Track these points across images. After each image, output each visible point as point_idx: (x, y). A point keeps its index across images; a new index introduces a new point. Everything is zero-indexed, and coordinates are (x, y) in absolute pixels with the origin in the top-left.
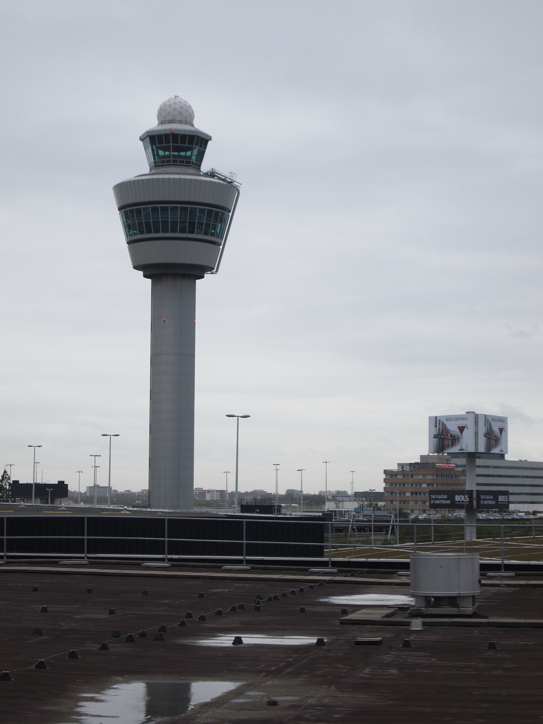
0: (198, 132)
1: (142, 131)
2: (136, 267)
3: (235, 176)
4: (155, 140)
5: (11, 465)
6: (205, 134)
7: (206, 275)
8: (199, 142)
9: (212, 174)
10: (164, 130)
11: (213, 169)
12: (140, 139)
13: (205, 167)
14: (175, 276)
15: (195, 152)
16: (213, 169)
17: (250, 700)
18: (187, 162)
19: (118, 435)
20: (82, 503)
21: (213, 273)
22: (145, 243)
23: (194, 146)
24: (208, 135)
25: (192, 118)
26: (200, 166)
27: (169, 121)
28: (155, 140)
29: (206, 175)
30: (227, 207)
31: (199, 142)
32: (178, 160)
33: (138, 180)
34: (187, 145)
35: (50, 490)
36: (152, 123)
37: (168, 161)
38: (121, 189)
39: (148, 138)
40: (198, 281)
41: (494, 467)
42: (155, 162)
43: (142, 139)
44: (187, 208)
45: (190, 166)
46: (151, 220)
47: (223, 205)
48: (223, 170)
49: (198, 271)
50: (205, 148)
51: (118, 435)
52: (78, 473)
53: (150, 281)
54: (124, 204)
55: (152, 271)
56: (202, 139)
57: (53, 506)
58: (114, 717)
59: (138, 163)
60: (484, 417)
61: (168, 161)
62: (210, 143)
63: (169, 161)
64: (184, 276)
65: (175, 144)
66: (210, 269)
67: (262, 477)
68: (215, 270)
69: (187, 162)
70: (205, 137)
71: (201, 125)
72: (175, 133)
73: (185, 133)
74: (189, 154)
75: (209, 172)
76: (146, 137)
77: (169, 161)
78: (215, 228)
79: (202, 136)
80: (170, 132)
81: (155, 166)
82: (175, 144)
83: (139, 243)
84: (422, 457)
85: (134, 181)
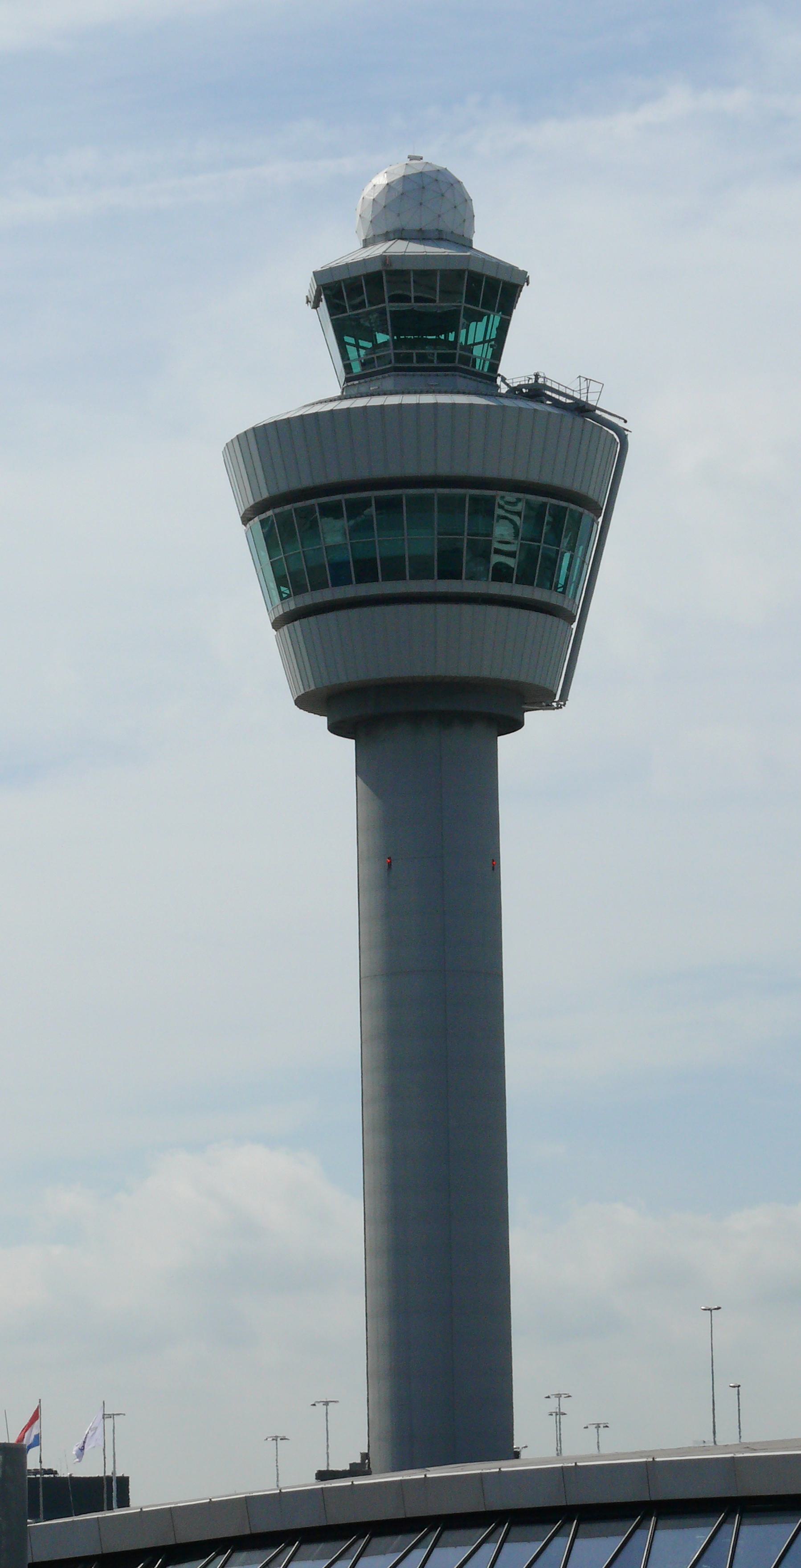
0: (487, 260)
2: (305, 702)
4: (346, 297)
6: (499, 265)
7: (529, 716)
8: (496, 292)
9: (535, 391)
11: (537, 376)
13: (515, 368)
14: (417, 718)
18: (442, 358)
22: (366, 611)
24: (512, 269)
25: (468, 218)
28: (346, 297)
29: (515, 392)
30: (590, 494)
31: (496, 292)
33: (316, 415)
36: (344, 244)
40: (503, 741)
45: (455, 369)
46: (465, 537)
48: (564, 379)
49: (504, 704)
51: (719, 1308)
52: (321, 1408)
53: (349, 745)
54: (275, 492)
55: (345, 704)
56: (493, 284)
64: (447, 719)
65: (418, 304)
66: (545, 698)
67: (582, 1448)
70: (504, 276)
71: (494, 239)
72: (397, 266)
73: (354, 274)
75: (525, 386)
78: (552, 563)
80: (378, 267)
82: (418, 304)
83: (331, 616)
85: (302, 417)
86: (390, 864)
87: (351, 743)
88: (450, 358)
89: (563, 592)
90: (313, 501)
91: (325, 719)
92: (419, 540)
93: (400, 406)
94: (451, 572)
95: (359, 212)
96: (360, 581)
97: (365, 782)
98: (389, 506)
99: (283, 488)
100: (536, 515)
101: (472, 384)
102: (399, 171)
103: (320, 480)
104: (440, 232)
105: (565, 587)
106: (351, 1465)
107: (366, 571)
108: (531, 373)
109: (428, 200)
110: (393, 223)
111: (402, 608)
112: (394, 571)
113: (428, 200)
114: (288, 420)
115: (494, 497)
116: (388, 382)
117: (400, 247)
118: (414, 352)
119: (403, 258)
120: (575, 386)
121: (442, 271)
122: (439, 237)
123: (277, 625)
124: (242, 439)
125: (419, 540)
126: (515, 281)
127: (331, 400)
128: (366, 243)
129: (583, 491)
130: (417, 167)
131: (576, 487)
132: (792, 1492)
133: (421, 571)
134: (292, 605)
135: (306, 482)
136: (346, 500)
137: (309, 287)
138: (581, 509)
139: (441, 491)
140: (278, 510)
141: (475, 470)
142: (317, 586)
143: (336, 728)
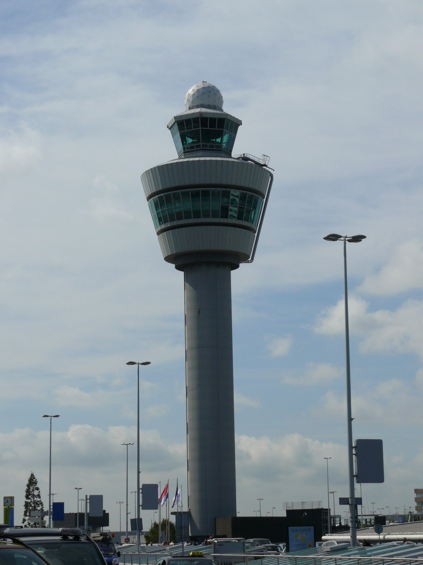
0: (227, 114)
1: (169, 119)
2: (168, 259)
3: (268, 158)
5: (120, 503)
10: (193, 114)
12: (168, 127)
13: (237, 151)
15: (226, 138)
16: (244, 154)
18: (210, 146)
20: (172, 543)
21: (248, 262)
23: (252, 209)
25: (221, 102)
26: (231, 151)
27: (197, 105)
34: (216, 129)
37: (197, 146)
42: (184, 148)
47: (257, 188)
48: (256, 154)
49: (235, 258)
50: (236, 133)
53: (182, 273)
54: (165, 187)
55: (180, 259)
57: (352, 528)
59: (167, 150)
60: (291, 548)
61: (197, 146)
62: (240, 127)
63: (199, 146)
65: (206, 128)
68: (250, 259)
71: (228, 109)
72: (204, 116)
74: (219, 140)
76: (174, 124)
77: (199, 146)
79: (232, 120)
80: (198, 116)
82: (206, 128)
86: (199, 312)
87: (182, 273)
88: (213, 146)
89: (252, 223)
90: (189, 190)
91: (174, 265)
92: (215, 205)
93: (199, 161)
94: (225, 216)
95: (187, 98)
96: (213, 217)
97: (190, 284)
98: (206, 194)
99: (168, 186)
100: (243, 198)
101: (223, 155)
102: (201, 85)
103: (173, 185)
104: (215, 106)
105: (253, 221)
106: (141, 519)
107: (197, 215)
108: (242, 154)
109: (209, 95)
110: (199, 102)
111: (209, 227)
112: (206, 215)
113: (209, 95)
114: (172, 164)
115: (230, 191)
116: (200, 153)
117: (204, 110)
118: (208, 144)
119: (206, 113)
120: (261, 157)
121: (218, 118)
122: (214, 108)
123: (158, 234)
124: (153, 171)
125: (215, 205)
126: (238, 123)
127: (176, 159)
128: (190, 108)
129: (259, 189)
130: (206, 85)
131: (257, 189)
132: (238, 509)
133: (215, 216)
134: (163, 227)
135: (177, 184)
136: (181, 192)
137: (169, 122)
138: (258, 196)
139: (223, 189)
140: (159, 195)
141: (224, 182)
142: (172, 220)
143: (178, 268)
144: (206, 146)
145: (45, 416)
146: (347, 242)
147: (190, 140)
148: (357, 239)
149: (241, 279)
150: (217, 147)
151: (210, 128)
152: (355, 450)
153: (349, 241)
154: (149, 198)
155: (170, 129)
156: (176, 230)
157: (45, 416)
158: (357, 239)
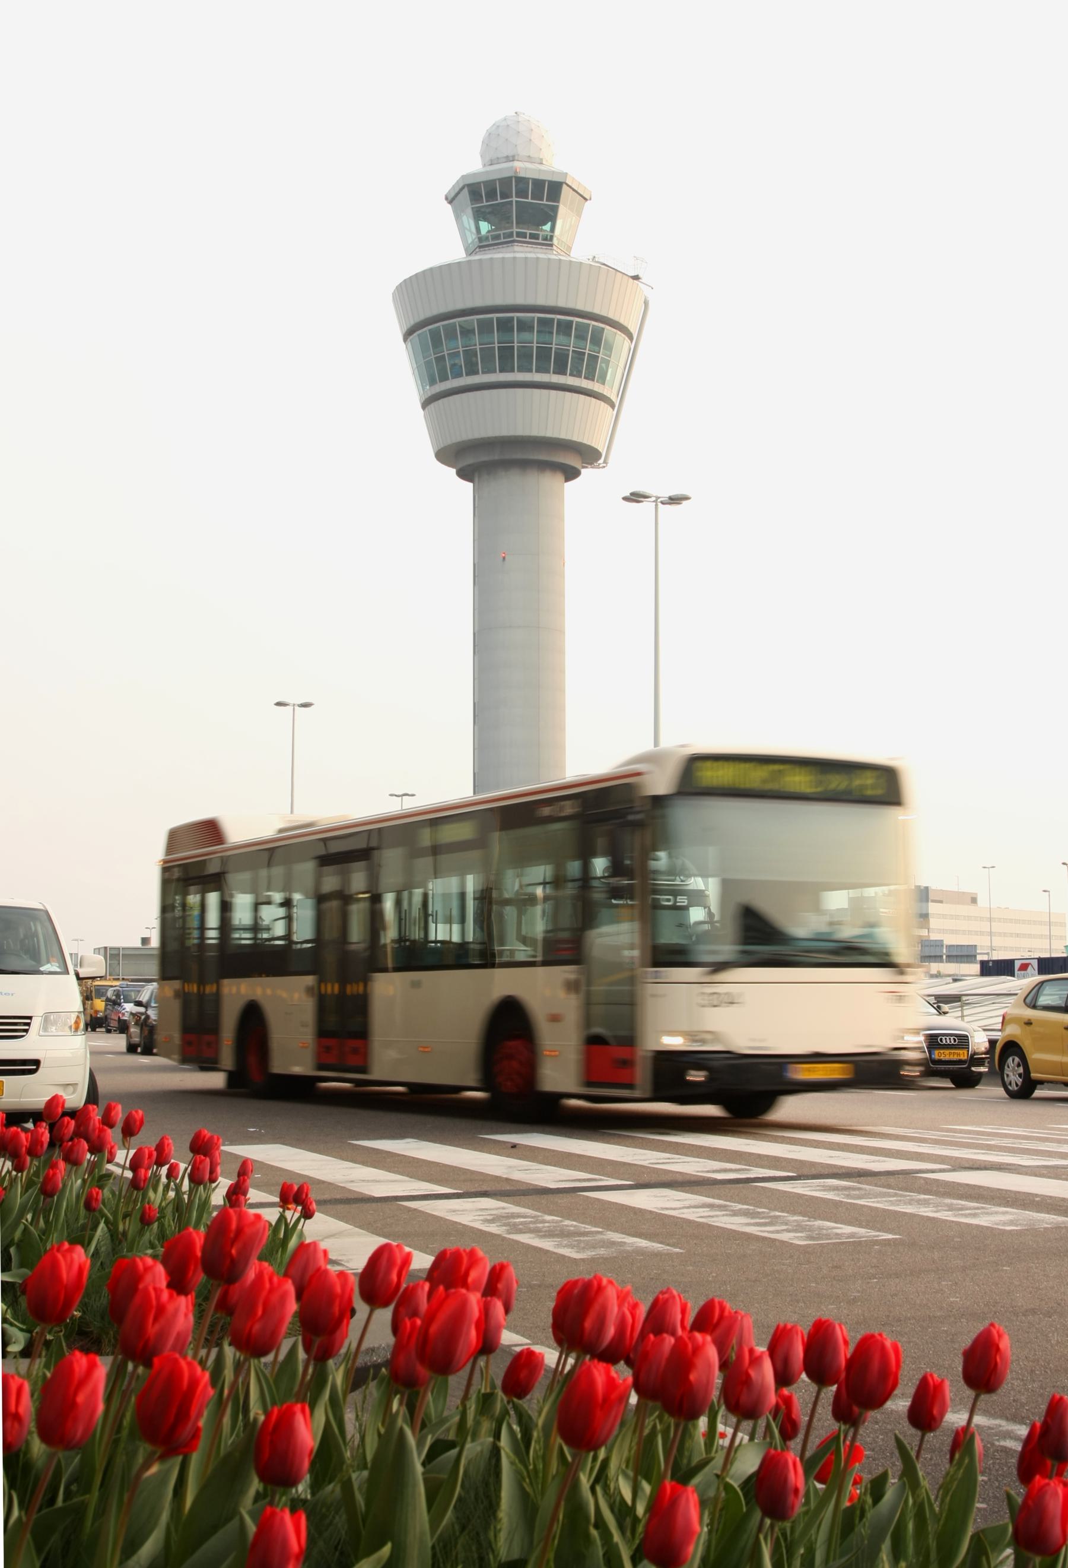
1: (449, 181)
12: (446, 199)
17: (563, 1503)
19: (391, 795)
32: (528, 232)
34: (545, 202)
35: (777, 1243)
36: (471, 164)
38: (410, 290)
39: (466, 190)
41: (1011, 935)
43: (451, 200)
44: (553, 320)
49: (566, 458)
51: (391, 795)
53: (469, 486)
55: (479, 459)
56: (539, 184)
58: (368, 1181)
59: (443, 239)
65: (513, 203)
69: (532, 236)
72: (522, 175)
73: (542, 177)
81: (480, 247)
82: (513, 203)
84: (314, 1244)
87: (471, 485)
121: (499, 180)
123: (425, 404)
124: (399, 288)
129: (625, 324)
143: (464, 474)
144: (524, 235)
145: (279, 704)
146: (660, 505)
147: (485, 227)
148: (675, 500)
149: (582, 504)
150: (545, 239)
151: (502, 198)
152: (308, 1518)
153: (662, 503)
154: (408, 334)
155: (450, 202)
156: (440, 401)
157: (279, 704)
158: (675, 500)
